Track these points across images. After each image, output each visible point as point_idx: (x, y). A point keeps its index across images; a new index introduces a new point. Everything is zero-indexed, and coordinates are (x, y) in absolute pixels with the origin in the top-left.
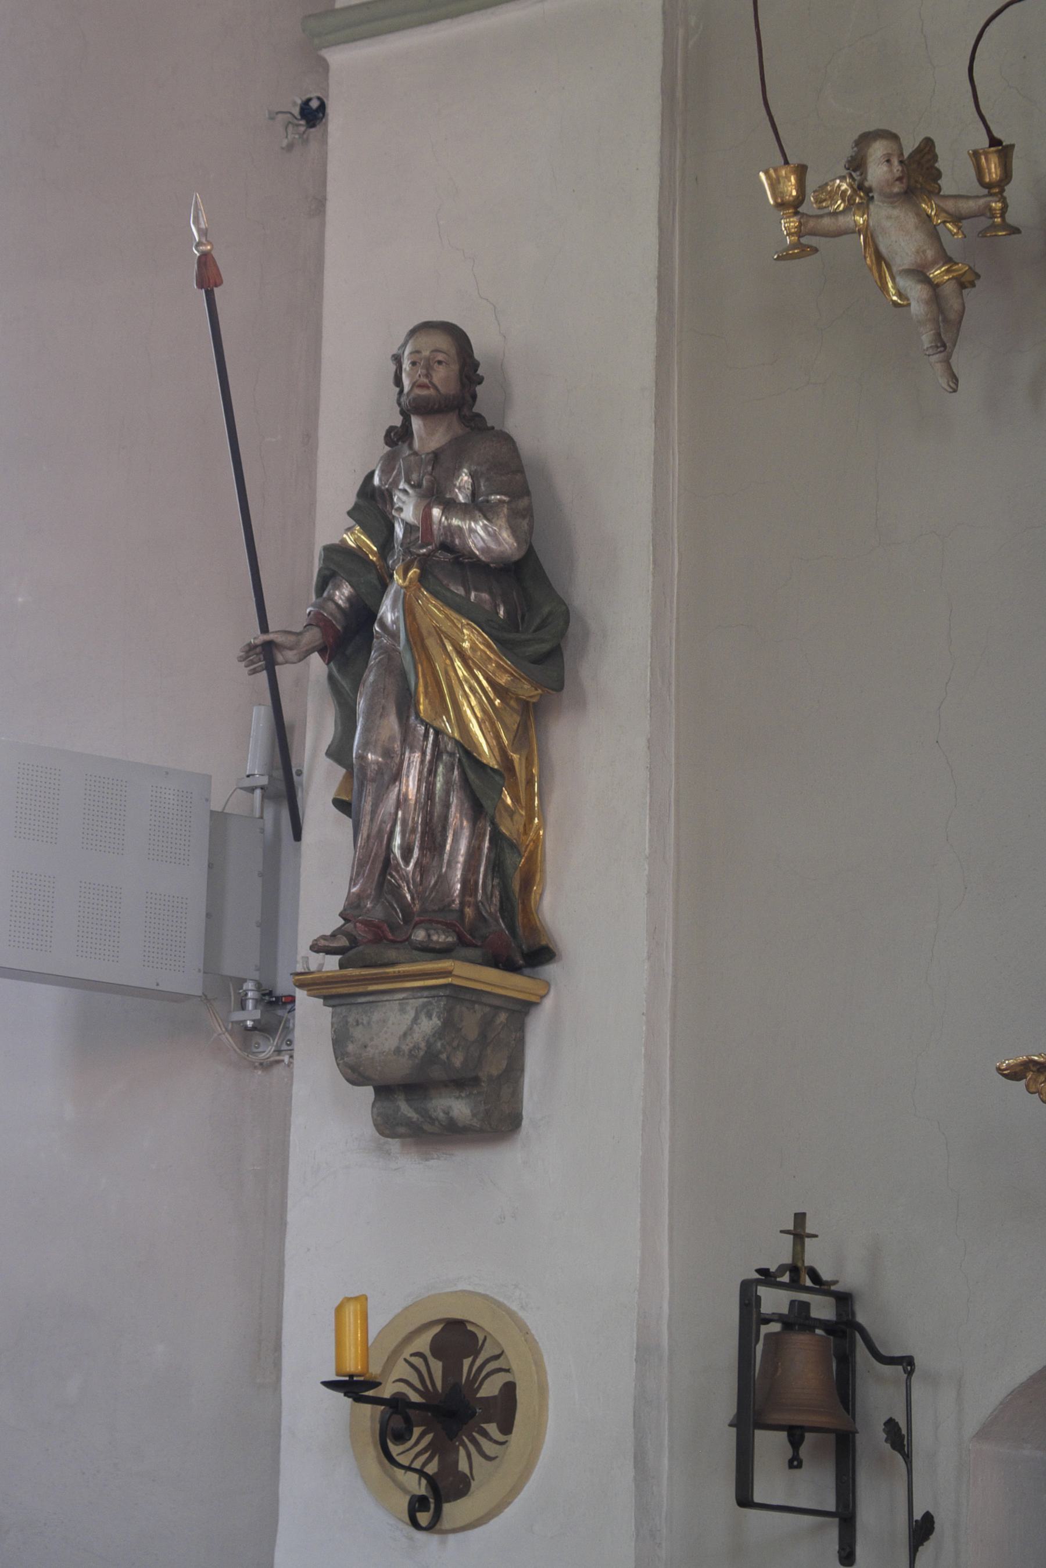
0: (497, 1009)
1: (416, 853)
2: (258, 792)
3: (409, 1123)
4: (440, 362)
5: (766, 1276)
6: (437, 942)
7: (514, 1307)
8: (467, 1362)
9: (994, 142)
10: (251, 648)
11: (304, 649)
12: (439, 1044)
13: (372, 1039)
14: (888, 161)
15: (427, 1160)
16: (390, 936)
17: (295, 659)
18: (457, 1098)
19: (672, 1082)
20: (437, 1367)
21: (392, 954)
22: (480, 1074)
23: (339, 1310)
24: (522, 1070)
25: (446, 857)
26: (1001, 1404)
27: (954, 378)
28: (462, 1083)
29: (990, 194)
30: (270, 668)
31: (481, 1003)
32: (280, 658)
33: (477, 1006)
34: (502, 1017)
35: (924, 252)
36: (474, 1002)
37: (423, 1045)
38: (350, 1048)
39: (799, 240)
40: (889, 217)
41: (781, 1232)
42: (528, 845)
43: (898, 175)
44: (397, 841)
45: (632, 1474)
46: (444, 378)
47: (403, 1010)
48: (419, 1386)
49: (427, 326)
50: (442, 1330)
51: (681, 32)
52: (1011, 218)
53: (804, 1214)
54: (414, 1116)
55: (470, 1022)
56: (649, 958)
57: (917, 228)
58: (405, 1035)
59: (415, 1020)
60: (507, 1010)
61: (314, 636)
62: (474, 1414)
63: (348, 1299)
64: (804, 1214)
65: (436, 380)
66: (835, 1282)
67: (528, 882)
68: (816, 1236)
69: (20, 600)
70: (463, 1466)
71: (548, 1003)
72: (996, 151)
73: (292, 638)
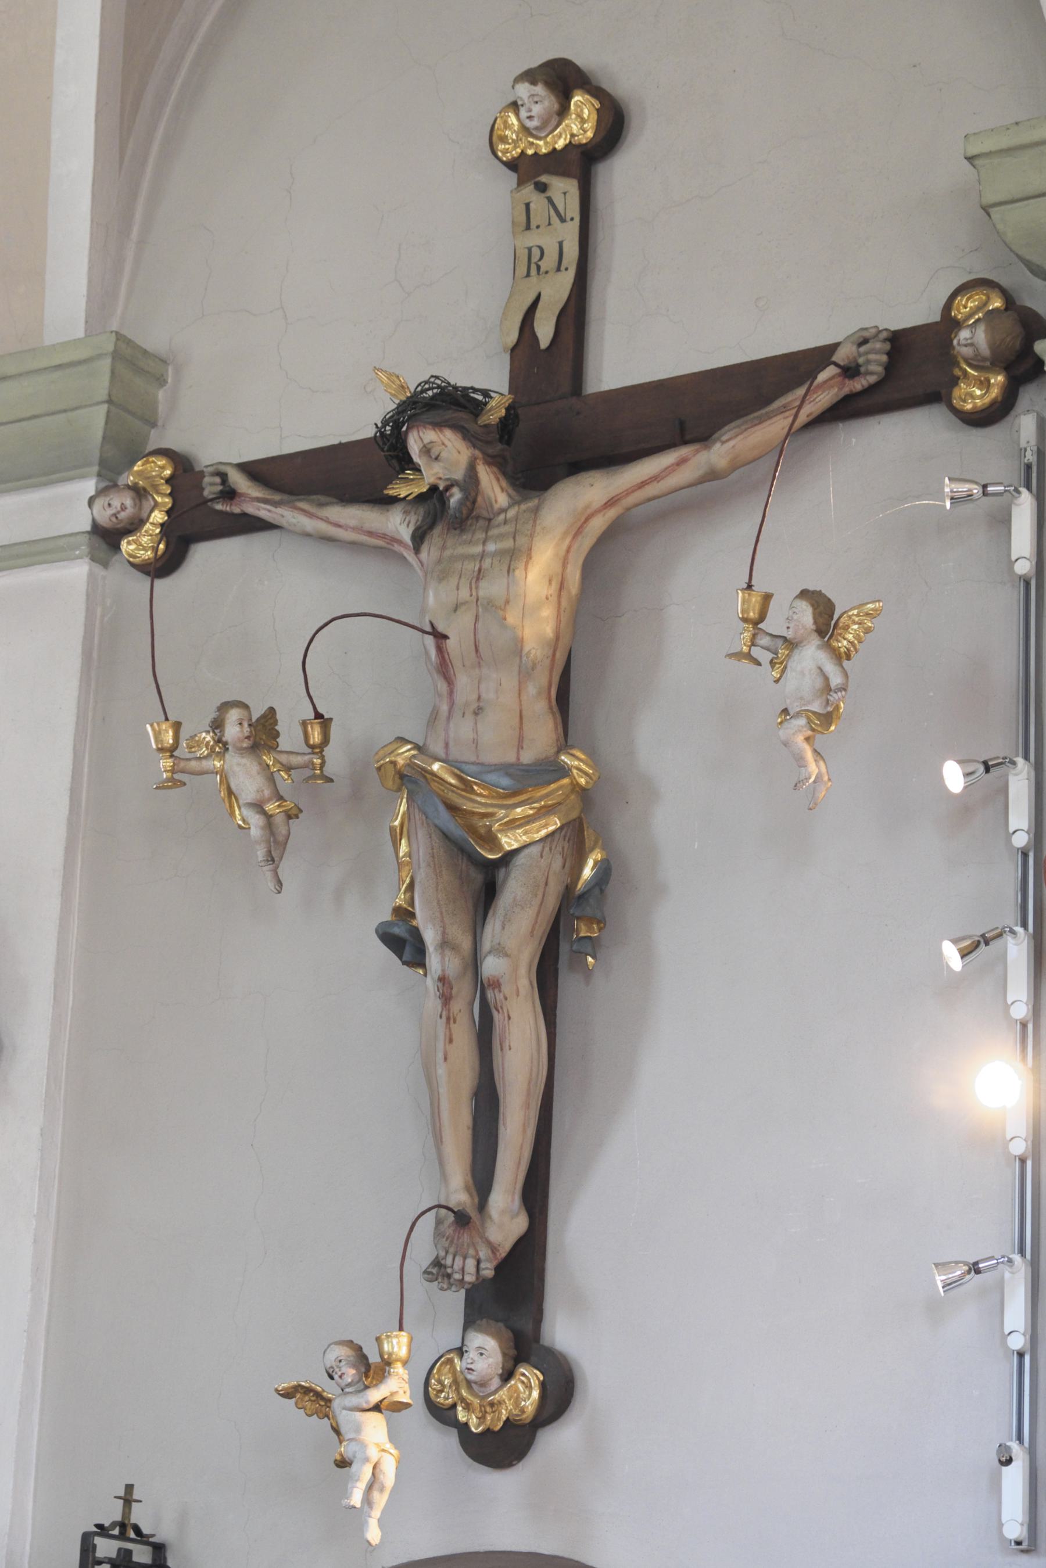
5: (102, 1530)
9: (318, 716)
14: (240, 724)
27: (280, 883)
35: (262, 791)
43: (247, 734)
52: (328, 770)
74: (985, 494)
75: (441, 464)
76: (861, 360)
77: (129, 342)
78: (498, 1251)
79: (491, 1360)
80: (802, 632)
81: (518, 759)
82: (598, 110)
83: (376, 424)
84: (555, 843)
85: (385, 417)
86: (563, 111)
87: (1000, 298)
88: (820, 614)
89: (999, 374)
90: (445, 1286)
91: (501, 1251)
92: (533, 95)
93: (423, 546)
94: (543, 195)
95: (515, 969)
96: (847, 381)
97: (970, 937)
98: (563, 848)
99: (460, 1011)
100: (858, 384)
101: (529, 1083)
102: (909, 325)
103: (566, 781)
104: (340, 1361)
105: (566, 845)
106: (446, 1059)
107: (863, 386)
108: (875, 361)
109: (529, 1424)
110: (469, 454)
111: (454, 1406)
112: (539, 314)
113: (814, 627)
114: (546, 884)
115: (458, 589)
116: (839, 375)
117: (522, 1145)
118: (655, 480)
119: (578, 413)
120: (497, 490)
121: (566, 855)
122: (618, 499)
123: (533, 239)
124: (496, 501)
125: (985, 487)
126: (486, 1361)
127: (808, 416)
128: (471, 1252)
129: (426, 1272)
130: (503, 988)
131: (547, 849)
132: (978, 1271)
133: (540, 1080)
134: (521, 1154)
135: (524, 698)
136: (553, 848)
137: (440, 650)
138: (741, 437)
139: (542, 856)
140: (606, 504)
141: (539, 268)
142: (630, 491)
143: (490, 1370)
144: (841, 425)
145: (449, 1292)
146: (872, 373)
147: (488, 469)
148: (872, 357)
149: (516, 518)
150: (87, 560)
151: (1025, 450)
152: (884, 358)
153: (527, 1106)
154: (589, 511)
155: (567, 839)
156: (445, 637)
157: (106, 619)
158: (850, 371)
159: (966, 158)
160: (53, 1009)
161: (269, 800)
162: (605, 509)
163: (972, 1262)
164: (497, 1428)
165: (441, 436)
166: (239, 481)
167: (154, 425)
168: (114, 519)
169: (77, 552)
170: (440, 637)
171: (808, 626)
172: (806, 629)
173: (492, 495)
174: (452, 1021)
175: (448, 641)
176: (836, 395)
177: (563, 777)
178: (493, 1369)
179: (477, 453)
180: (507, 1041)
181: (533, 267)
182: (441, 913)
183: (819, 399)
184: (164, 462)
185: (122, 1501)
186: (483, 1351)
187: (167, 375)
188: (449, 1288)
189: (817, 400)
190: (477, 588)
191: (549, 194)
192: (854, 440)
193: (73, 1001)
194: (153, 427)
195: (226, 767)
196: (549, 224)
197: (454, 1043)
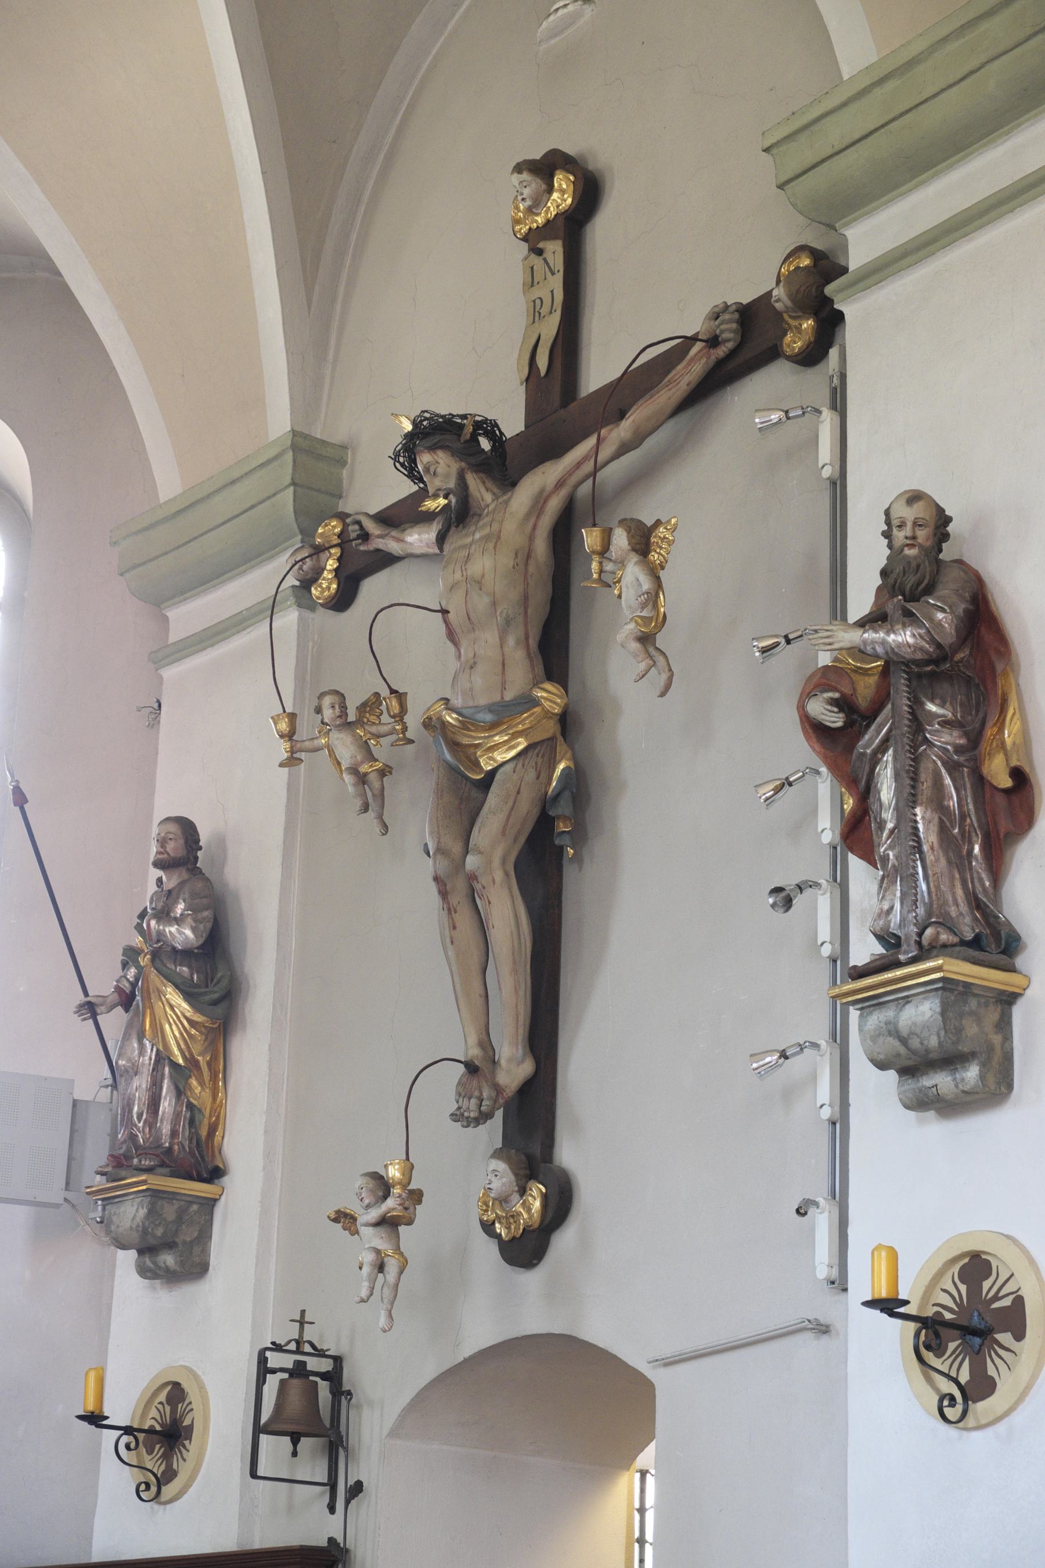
0: (191, 1203)
1: (144, 1117)
2: (110, 1088)
3: (150, 1270)
4: (171, 839)
5: (277, 1347)
6: (144, 1165)
7: (200, 1373)
8: (180, 1406)
9: (393, 691)
10: (81, 1006)
11: (110, 1005)
12: (147, 1224)
13: (120, 1222)
14: (333, 707)
15: (171, 1292)
16: (126, 1164)
17: (105, 1011)
18: (169, 1254)
19: (278, 1240)
20: (168, 1409)
21: (123, 1173)
22: (177, 1240)
23: (87, 1373)
24: (211, 1237)
25: (160, 1117)
26: (399, 1416)
27: (385, 827)
28: (169, 1245)
29: (396, 722)
30: (94, 1016)
31: (177, 1200)
32: (98, 1011)
33: (174, 1201)
34: (195, 1207)
35: (355, 757)
36: (172, 1199)
37: (141, 1224)
38: (113, 1228)
39: (292, 755)
40: (338, 739)
41: (290, 1321)
42: (216, 1109)
43: (338, 714)
44: (136, 1109)
45: (240, 1465)
46: (175, 848)
47: (132, 1205)
48: (160, 1421)
49: (168, 819)
50: (172, 1388)
51: (311, 644)
52: (409, 734)
53: (305, 1310)
54: (151, 1265)
55: (170, 1212)
56: (264, 1170)
57: (352, 743)
58: (133, 1219)
59: (137, 1211)
60: (197, 1203)
61: (115, 997)
62: (181, 1435)
63: (91, 1369)
64: (305, 1310)
65: (168, 850)
66: (328, 1350)
67: (213, 1129)
68: (313, 1323)
69: (22, 989)
70: (175, 1466)
71: (223, 1198)
72: (395, 696)
73: (101, 999)
74: (788, 418)
75: (438, 478)
76: (718, 332)
77: (306, 437)
78: (505, 1091)
79: (504, 1180)
80: (620, 553)
81: (502, 698)
82: (573, 183)
83: (390, 457)
84: (528, 760)
85: (395, 450)
86: (550, 189)
87: (808, 258)
88: (633, 536)
89: (808, 319)
90: (465, 1124)
91: (507, 1092)
92: (521, 182)
93: (445, 545)
94: (541, 258)
95: (489, 862)
96: (712, 351)
97: (779, 779)
98: (536, 763)
99: (459, 903)
100: (721, 351)
101: (513, 954)
102: (756, 296)
103: (537, 710)
104: (362, 1188)
105: (540, 761)
106: (452, 943)
107: (724, 352)
108: (727, 330)
109: (538, 1228)
110: (458, 467)
111: (493, 1223)
112: (539, 350)
113: (629, 548)
114: (518, 793)
115: (454, 573)
116: (705, 347)
117: (516, 1004)
118: (586, 460)
119: (564, 421)
120: (483, 490)
121: (540, 768)
122: (565, 480)
123: (536, 293)
124: (483, 500)
125: (787, 412)
126: (500, 1181)
127: (688, 385)
128: (476, 1093)
129: (452, 1115)
130: (479, 880)
131: (520, 765)
132: (786, 1058)
133: (523, 949)
134: (517, 1011)
135: (506, 649)
136: (526, 763)
137: (446, 622)
138: (638, 411)
139: (514, 772)
140: (556, 486)
141: (540, 313)
142: (571, 472)
143: (504, 1188)
144: (728, 388)
145: (470, 1129)
146: (728, 340)
147: (475, 476)
148: (723, 327)
149: (494, 510)
150: (295, 607)
151: (833, 376)
152: (734, 326)
153: (515, 971)
154: (545, 494)
155: (540, 755)
156: (448, 612)
157: (315, 649)
158: (713, 342)
159: (763, 151)
160: (277, 952)
161: (362, 762)
162: (557, 489)
163: (781, 1049)
164: (518, 1236)
165: (435, 457)
166: (370, 526)
167: (340, 497)
168: (301, 572)
169: (289, 603)
170: (444, 612)
171: (624, 548)
172: (623, 550)
173: (478, 495)
174: (453, 913)
175: (449, 614)
176: (706, 363)
177: (535, 707)
178: (507, 1187)
179: (463, 464)
180: (490, 921)
181: (537, 314)
182: (438, 827)
183: (693, 369)
184: (335, 523)
185: (298, 1324)
186: (497, 1173)
187: (347, 458)
188: (467, 1126)
189: (692, 371)
190: (466, 569)
191: (545, 255)
192: (736, 398)
193: (296, 943)
194: (340, 498)
195: (330, 742)
196: (545, 279)
197: (458, 929)
